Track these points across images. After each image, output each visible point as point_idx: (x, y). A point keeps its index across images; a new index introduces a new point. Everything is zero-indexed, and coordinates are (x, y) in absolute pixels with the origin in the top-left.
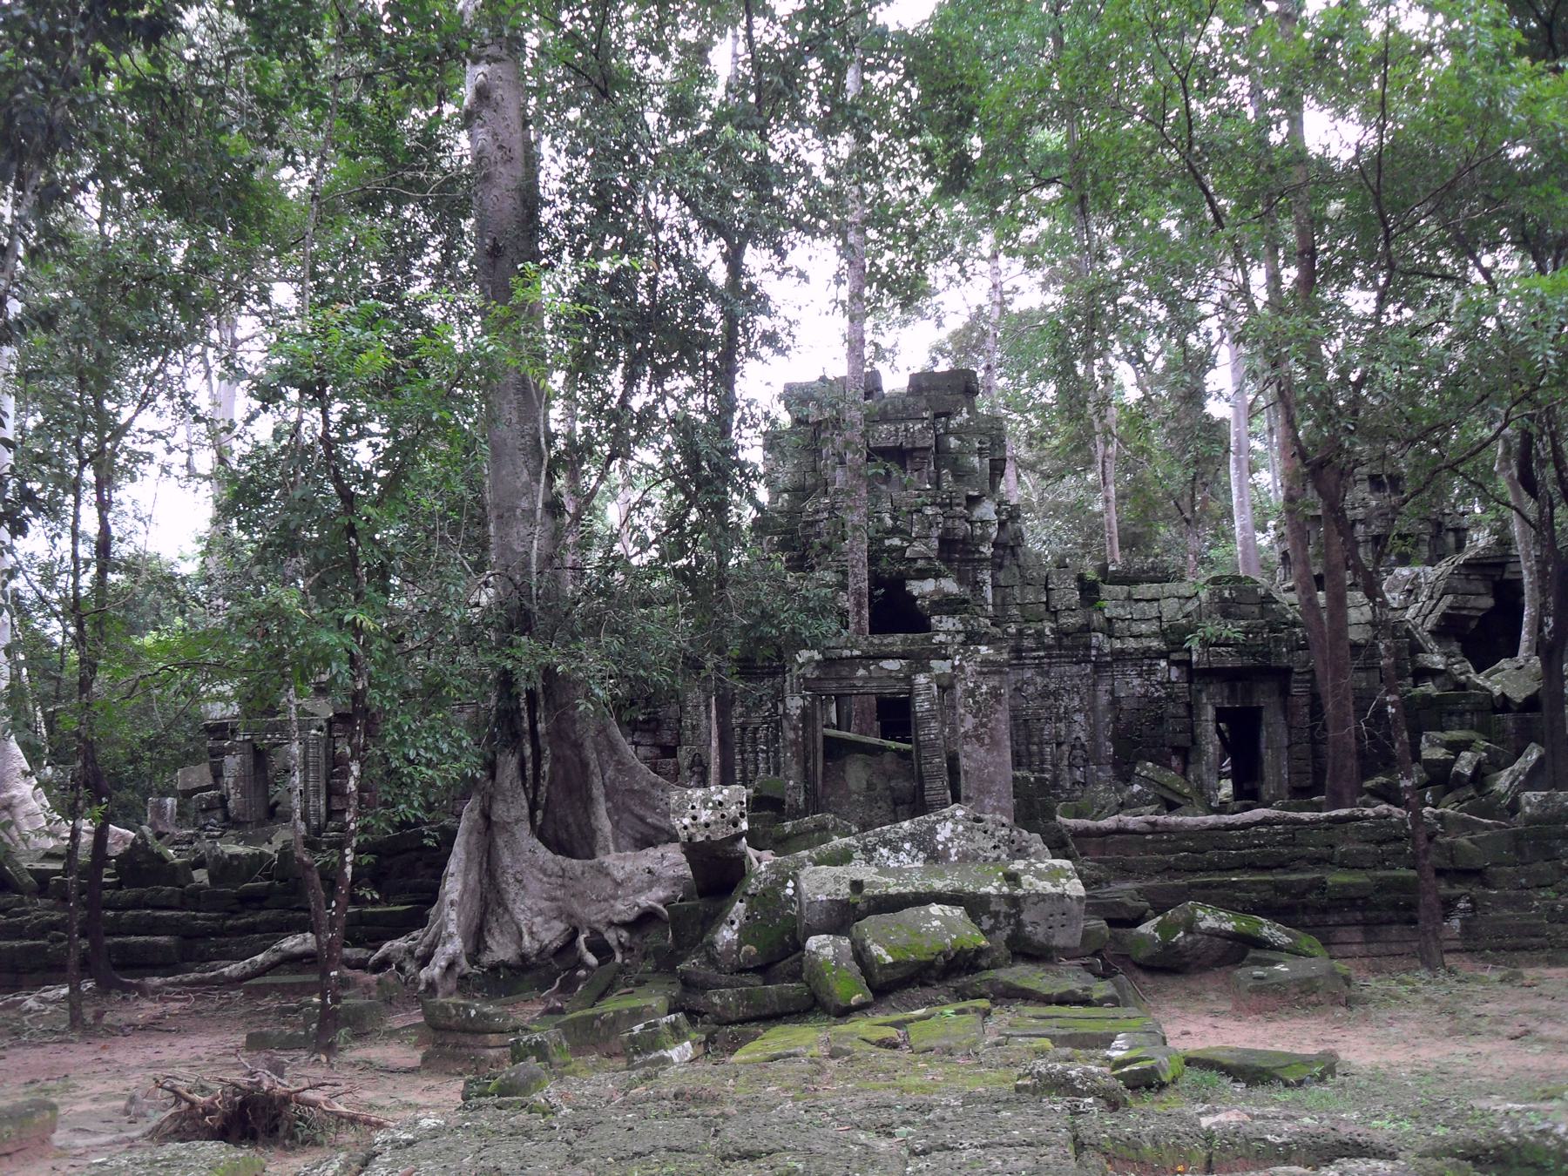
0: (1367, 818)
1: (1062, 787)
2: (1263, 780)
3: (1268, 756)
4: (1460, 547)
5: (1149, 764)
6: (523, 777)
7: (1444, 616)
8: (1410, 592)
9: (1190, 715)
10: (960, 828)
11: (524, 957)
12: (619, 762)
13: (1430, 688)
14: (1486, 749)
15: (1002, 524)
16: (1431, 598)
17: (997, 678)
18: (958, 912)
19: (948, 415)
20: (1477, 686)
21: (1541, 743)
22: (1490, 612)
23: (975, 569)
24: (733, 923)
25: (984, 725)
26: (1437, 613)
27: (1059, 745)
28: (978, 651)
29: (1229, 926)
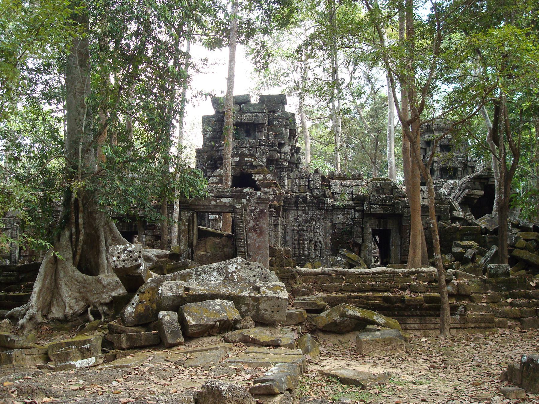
0: (424, 272)
1: (311, 258)
2: (390, 257)
3: (393, 248)
4: (473, 172)
5: (345, 250)
6: (71, 241)
7: (464, 197)
8: (452, 188)
9: (362, 231)
10: (239, 267)
11: (65, 316)
12: (114, 237)
13: (456, 224)
14: (478, 249)
15: (292, 155)
16: (460, 190)
17: (264, 205)
18: (230, 303)
19: (274, 112)
20: (476, 224)
21: (497, 245)
22: (483, 196)
23: (281, 172)
24: (133, 304)
25: (257, 225)
26: (462, 196)
27: (311, 241)
28: (256, 194)
29: (358, 314)
